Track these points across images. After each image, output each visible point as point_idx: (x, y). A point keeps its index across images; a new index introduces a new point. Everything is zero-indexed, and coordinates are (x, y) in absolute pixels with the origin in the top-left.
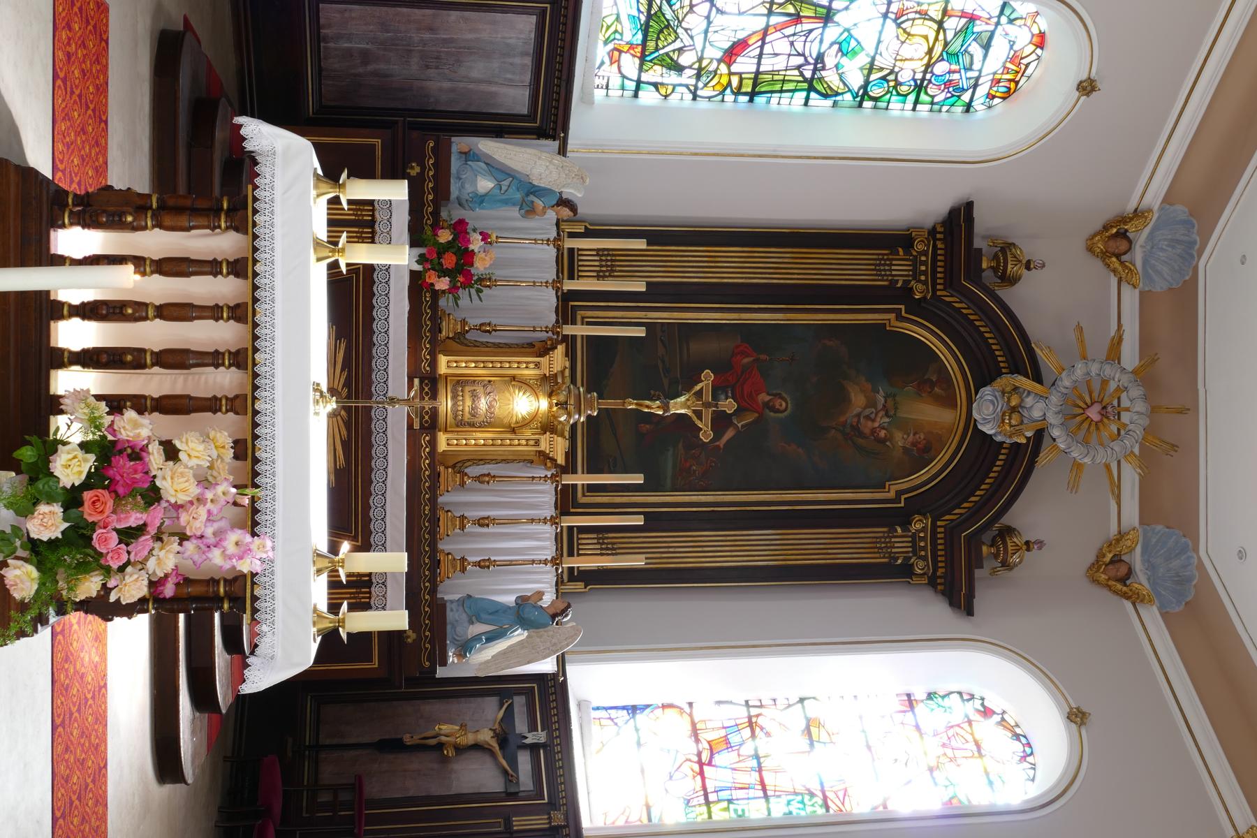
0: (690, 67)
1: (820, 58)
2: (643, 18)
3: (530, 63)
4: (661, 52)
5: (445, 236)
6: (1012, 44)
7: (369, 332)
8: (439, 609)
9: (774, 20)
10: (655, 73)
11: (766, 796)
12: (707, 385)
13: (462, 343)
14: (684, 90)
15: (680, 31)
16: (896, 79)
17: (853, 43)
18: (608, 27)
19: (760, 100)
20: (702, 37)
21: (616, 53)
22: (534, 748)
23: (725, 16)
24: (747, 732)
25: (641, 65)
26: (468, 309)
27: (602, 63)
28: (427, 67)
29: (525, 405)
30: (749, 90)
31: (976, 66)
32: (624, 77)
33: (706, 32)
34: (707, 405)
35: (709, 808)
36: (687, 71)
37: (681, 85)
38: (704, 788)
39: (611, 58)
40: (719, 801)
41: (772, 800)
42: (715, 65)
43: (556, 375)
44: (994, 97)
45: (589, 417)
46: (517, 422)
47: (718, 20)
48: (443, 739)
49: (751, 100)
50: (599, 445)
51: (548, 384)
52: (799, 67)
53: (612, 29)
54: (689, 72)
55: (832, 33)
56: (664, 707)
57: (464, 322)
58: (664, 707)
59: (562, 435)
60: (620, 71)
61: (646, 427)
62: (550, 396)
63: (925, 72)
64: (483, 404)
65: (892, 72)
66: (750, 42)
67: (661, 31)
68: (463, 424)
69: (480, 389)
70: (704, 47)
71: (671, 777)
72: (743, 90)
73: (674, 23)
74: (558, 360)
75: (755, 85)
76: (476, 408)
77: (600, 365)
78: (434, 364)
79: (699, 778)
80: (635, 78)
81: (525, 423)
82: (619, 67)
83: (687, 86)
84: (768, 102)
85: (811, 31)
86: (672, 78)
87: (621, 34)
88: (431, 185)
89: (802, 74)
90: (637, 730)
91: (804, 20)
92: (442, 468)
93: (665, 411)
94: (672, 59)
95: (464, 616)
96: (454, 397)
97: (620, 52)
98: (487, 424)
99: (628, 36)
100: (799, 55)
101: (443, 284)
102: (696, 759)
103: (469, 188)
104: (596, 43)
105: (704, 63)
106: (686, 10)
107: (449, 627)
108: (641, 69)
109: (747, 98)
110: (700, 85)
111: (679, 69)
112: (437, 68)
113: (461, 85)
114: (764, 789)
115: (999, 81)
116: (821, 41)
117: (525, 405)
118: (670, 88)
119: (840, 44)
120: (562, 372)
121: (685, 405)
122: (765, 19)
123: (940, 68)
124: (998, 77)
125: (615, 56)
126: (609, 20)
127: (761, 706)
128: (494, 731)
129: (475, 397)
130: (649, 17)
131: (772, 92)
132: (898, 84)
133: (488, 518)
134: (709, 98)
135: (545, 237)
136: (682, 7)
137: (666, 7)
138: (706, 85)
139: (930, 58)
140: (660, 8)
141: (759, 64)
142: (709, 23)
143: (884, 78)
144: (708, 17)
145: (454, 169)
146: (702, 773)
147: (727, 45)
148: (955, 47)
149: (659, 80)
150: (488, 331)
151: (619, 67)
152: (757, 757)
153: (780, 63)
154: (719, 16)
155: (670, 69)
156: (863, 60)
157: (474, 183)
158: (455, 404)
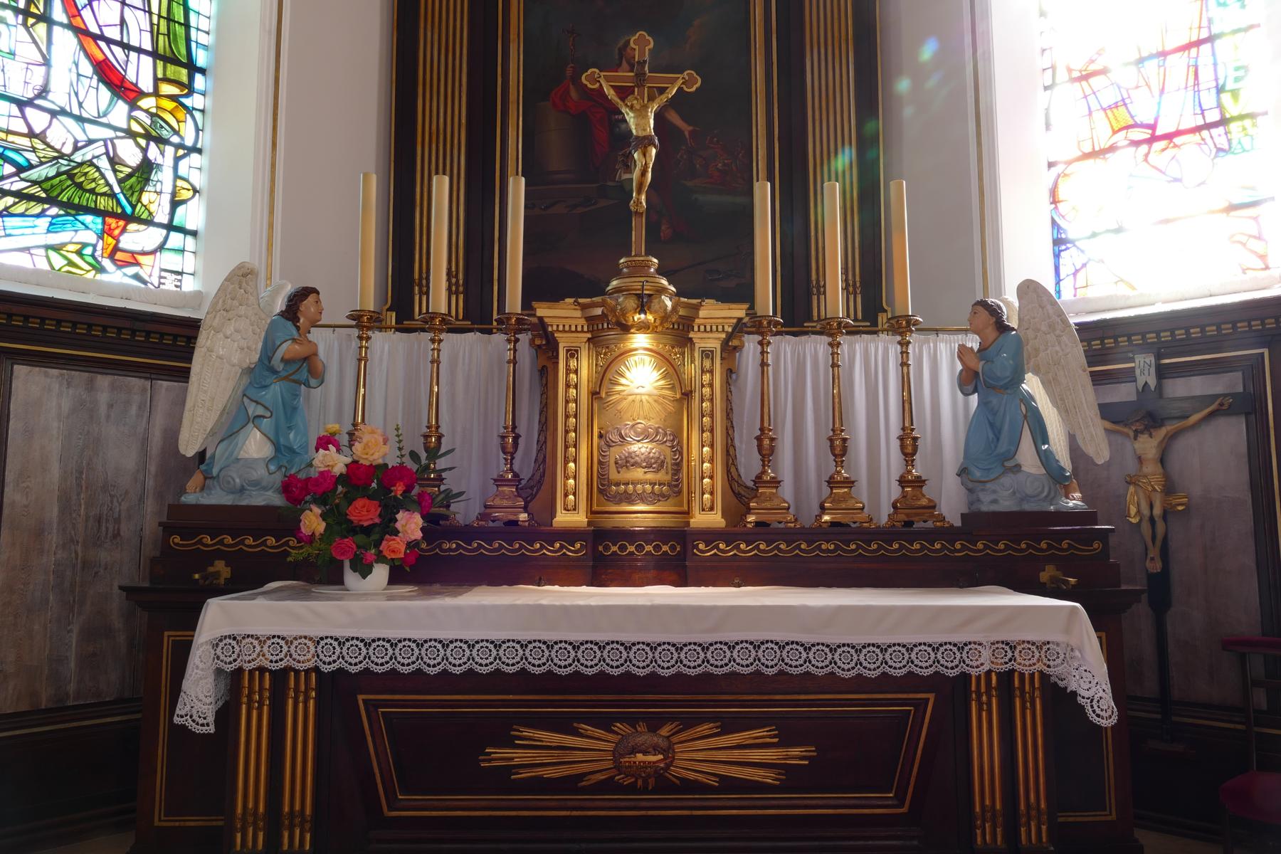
0: (145, 151)
2: (54, 211)
3: (165, 383)
4: (117, 189)
5: (313, 521)
7: (497, 680)
8: (978, 524)
10: (156, 202)
11: (1210, 39)
12: (608, 79)
13: (537, 488)
14: (183, 165)
15: (78, 157)
18: (71, 263)
19: (201, 59)
20: (89, 126)
21: (119, 256)
22: (1163, 373)
23: (53, 86)
24: (1095, 82)
25: (139, 221)
26: (471, 482)
27: (137, 277)
28: (117, 535)
29: (641, 375)
30: (184, 71)
32: (161, 247)
33: (80, 119)
34: (640, 79)
35: (1233, 119)
37: (175, 168)
38: (1198, 129)
39: (128, 264)
40: (1220, 106)
41: (1215, 31)
43: (590, 319)
45: (661, 271)
46: (673, 388)
47: (59, 97)
48: (1157, 511)
49: (203, 71)
50: (707, 258)
51: (605, 334)
56: (1055, 201)
57: (500, 481)
58: (1055, 201)
59: (697, 308)
60: (153, 252)
61: (665, 229)
62: (626, 329)
64: (640, 448)
66: (100, 57)
67: (80, 186)
68: (676, 484)
69: (615, 453)
70: (109, 126)
71: (1176, 180)
72: (185, 79)
73: (64, 165)
74: (562, 315)
75: (176, 61)
76: (647, 459)
77: (575, 262)
78: (570, 535)
79: (1177, 140)
80: (164, 232)
81: (672, 372)
82: (144, 253)
83: (177, 159)
84: (206, 47)
86: (164, 178)
87: (84, 245)
88: (250, 541)
90: (1094, 235)
92: (751, 518)
93: (652, 144)
94: (129, 176)
95: (1007, 480)
96: (629, 498)
97: (116, 249)
98: (676, 442)
99: (90, 237)
101: (411, 525)
102: (1144, 148)
103: (260, 473)
104: (100, 283)
105: (136, 128)
106: (39, 145)
107: (1028, 507)
108: (149, 222)
109: (198, 77)
110: (175, 139)
111: (146, 169)
112: (118, 521)
113: (150, 483)
114: (1198, 43)
117: (641, 375)
118: (180, 183)
120: (584, 307)
121: (641, 113)
126: (58, 262)
127: (1053, 68)
128: (1137, 433)
129: (628, 462)
130: (52, 201)
131: (188, 40)
133: (901, 439)
134: (197, 130)
135: (355, 343)
136: (34, 150)
137: (34, 174)
138: (177, 133)
140: (34, 183)
141: (140, 51)
142: (63, 112)
145: (227, 500)
146: (1169, 137)
147: (105, 93)
149: (166, 199)
150: (516, 438)
151: (144, 253)
152: (1141, 60)
154: (50, 96)
155: (147, 180)
157: (249, 463)
158: (642, 498)
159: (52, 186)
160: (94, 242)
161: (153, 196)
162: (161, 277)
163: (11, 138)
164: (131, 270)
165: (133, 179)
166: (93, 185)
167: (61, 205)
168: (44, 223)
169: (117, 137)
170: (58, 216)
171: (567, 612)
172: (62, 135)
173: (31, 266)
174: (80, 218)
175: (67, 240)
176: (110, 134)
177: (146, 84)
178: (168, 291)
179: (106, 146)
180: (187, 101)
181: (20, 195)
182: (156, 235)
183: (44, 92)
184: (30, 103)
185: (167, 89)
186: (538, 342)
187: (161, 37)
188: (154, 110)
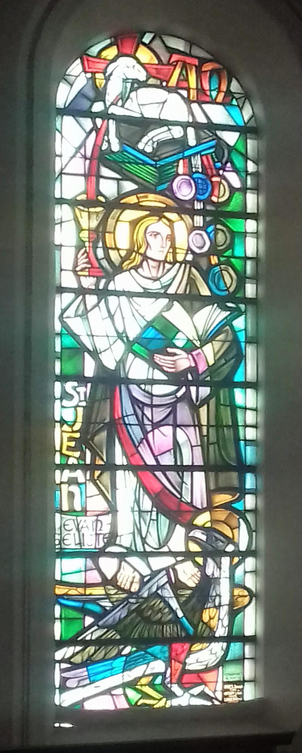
0: (202, 568)
1: (177, 378)
6: (137, 85)
9: (120, 459)
14: (239, 571)
16: (208, 255)
17: (151, 333)
18: (146, 695)
21: (186, 678)
30: (235, 475)
31: (177, 132)
36: (209, 572)
37: (232, 577)
42: (198, 534)
44: (229, 93)
47: (125, 540)
52: (195, 408)
53: (148, 690)
54: (211, 568)
55: (138, 369)
60: (216, 667)
63: (193, 213)
65: (194, 264)
66: (157, 487)
72: (236, 483)
75: (227, 468)
82: (207, 670)
83: (233, 568)
85: (134, 401)
86: (224, 590)
87: (155, 675)
89: (206, 401)
91: (118, 414)
94: (190, 597)
97: (184, 672)
100: (174, 412)
105: (194, 547)
108: (212, 639)
110: (230, 548)
115: (201, 90)
116: (153, 382)
118: (237, 592)
119: (152, 353)
122: (120, 473)
123: (185, 192)
124: (193, 93)
125: (190, 679)
126: (133, 695)
130: (125, 641)
131: (237, 440)
132: (214, 250)
136: (108, 596)
138: (230, 541)
139: (169, 209)
140: (109, 628)
142: (130, 552)
143: (205, 276)
144: (121, 557)
148: (146, 173)
149: (224, 610)
153: (187, 437)
156: (177, 315)
159: (125, 626)
160: (163, 670)
161: (213, 612)
162: (224, 691)
163: (88, 591)
164: (197, 690)
165: (194, 600)
166: (159, 615)
167: (133, 642)
168: (120, 662)
169: (177, 562)
170: (130, 653)
171: (118, 405)
172: (129, 575)
173: (112, 708)
174: (150, 650)
175: (140, 674)
176: (169, 561)
177: (200, 499)
178: (232, 704)
179: (168, 574)
180: (238, 506)
181: (99, 643)
182: (217, 648)
183: (112, 538)
184: (102, 552)
185: (222, 498)
186: (200, 598)
187: (211, 448)
188: (209, 525)
